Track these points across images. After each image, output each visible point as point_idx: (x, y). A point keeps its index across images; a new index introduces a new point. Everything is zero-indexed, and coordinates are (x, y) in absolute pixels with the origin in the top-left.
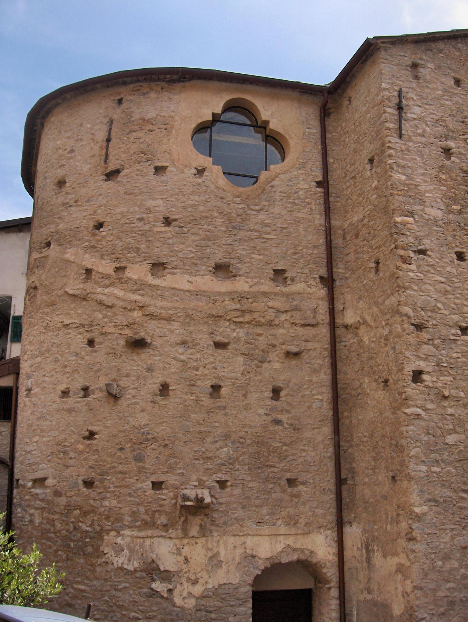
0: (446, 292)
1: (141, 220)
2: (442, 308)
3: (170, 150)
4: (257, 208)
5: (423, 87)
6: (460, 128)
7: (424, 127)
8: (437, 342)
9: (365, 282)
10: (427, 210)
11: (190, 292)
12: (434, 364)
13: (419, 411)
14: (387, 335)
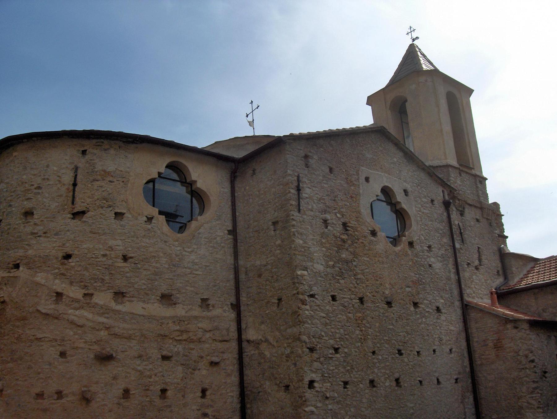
0: (326, 324)
1: (104, 255)
3: (127, 200)
4: (189, 250)
8: (322, 359)
9: (267, 312)
10: (316, 266)
11: (144, 316)
13: (313, 409)
14: (288, 354)
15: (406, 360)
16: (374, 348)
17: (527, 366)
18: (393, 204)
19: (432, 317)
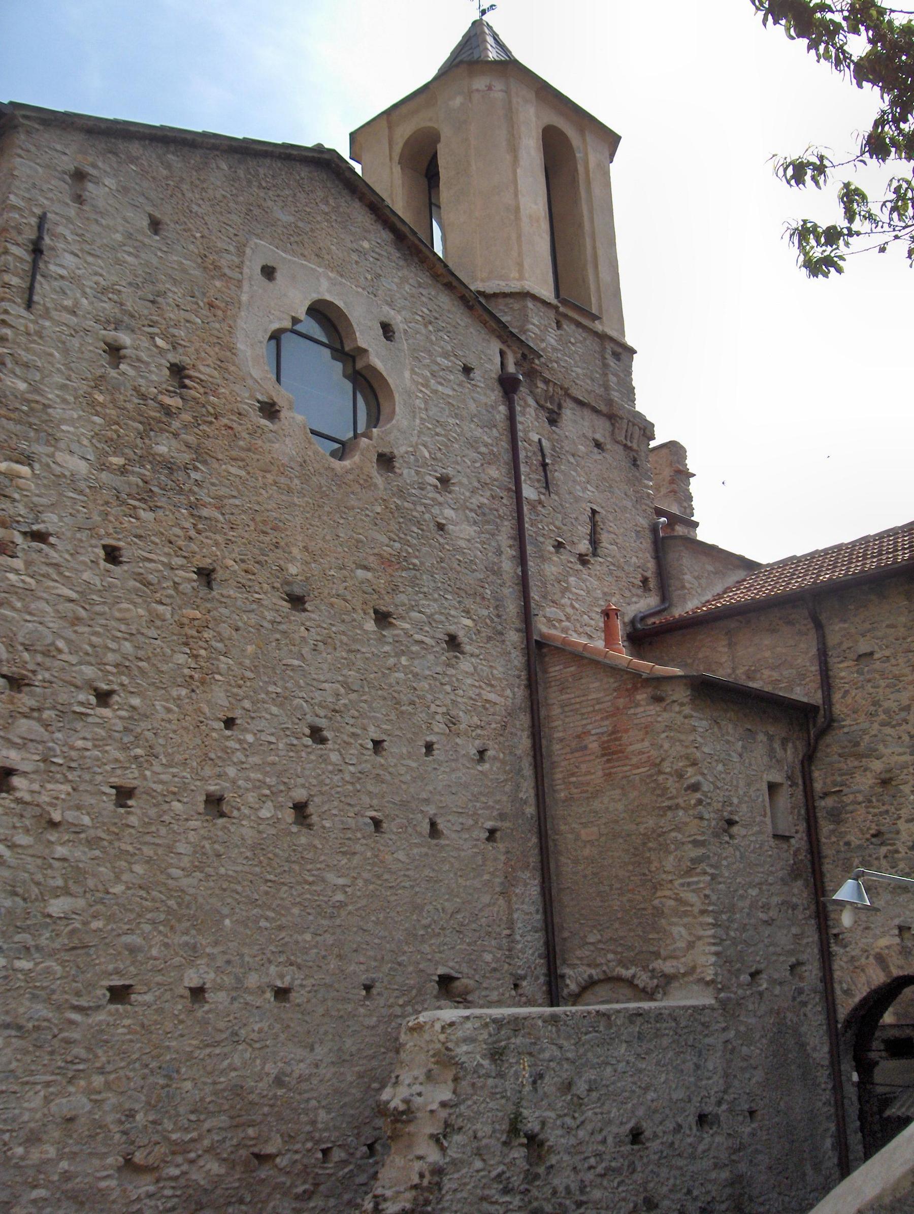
2: (66, 650)
5: (88, 219)
6: (146, 312)
7: (78, 295)
8: (47, 714)
10: (60, 457)
12: (38, 758)
15: (334, 757)
16: (232, 709)
17: (680, 801)
18: (347, 354)
19: (431, 657)
